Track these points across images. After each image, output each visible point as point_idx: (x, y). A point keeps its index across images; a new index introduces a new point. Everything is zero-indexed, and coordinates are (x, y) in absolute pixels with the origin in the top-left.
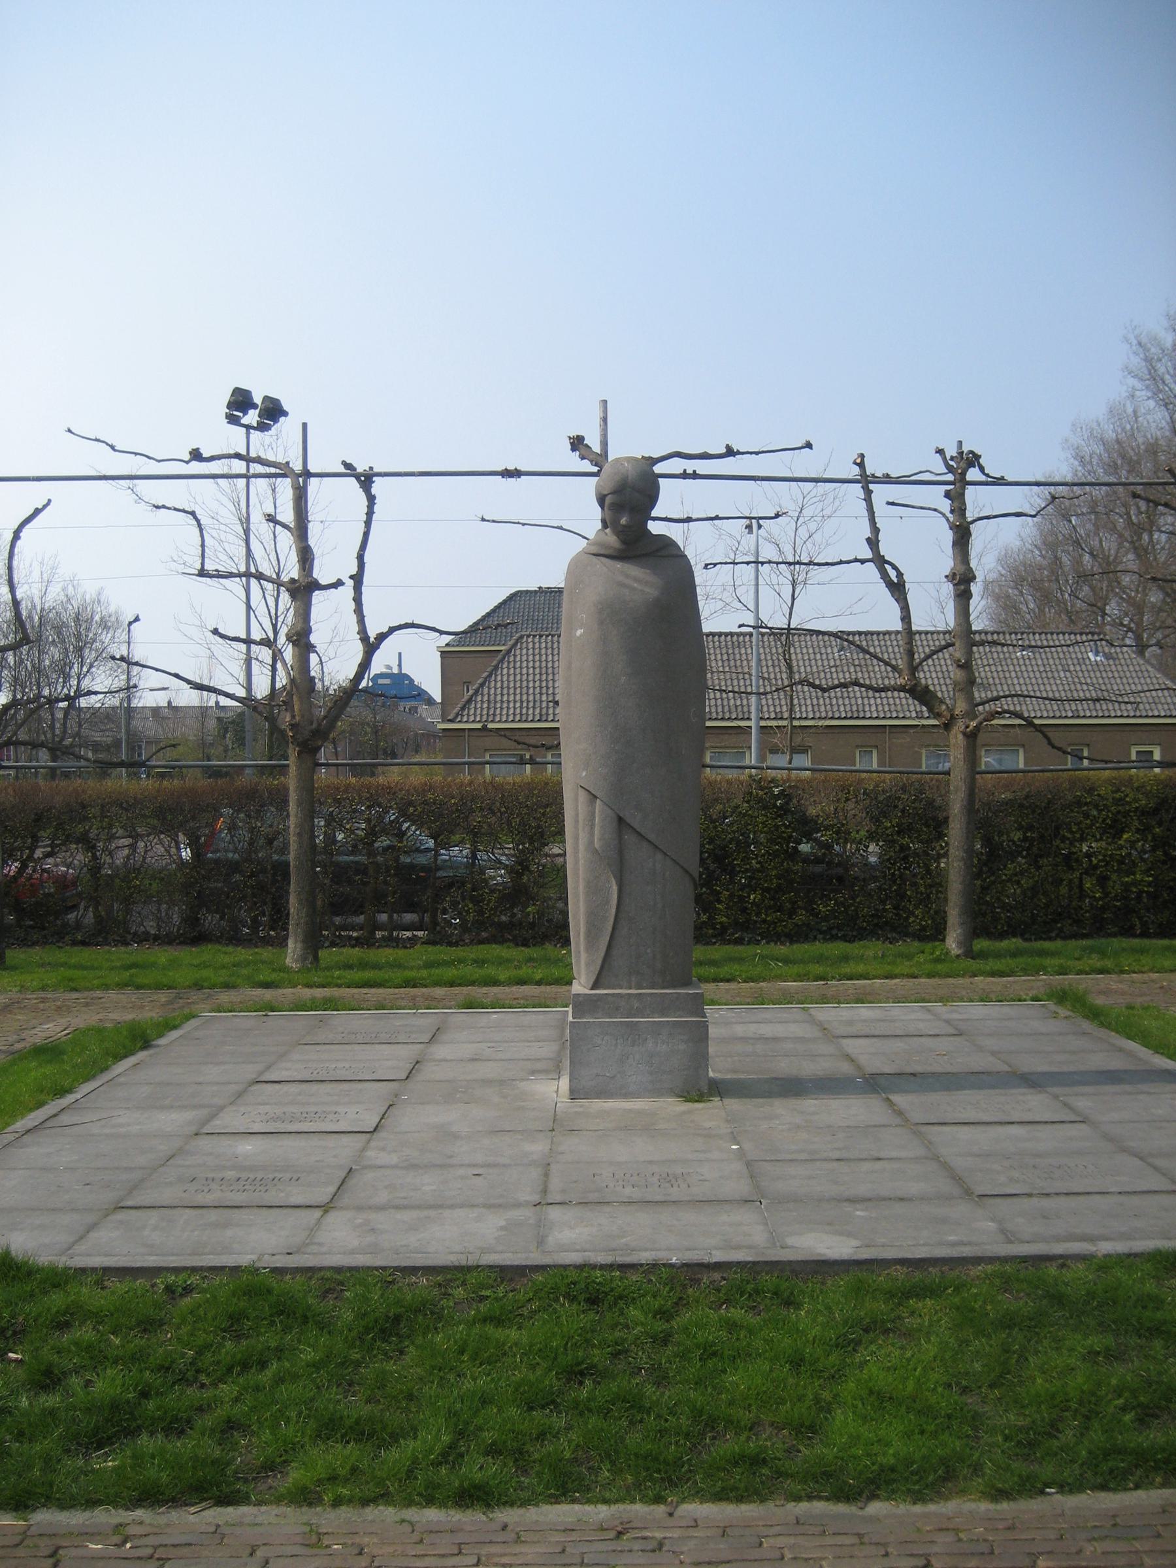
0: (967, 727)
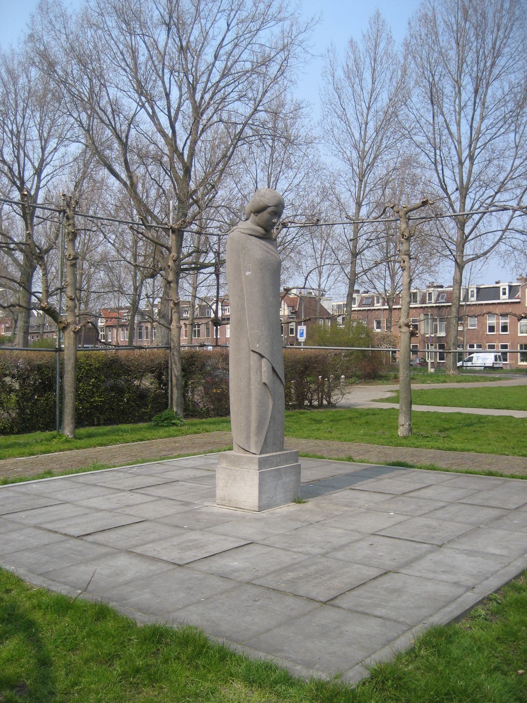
0: (76, 329)
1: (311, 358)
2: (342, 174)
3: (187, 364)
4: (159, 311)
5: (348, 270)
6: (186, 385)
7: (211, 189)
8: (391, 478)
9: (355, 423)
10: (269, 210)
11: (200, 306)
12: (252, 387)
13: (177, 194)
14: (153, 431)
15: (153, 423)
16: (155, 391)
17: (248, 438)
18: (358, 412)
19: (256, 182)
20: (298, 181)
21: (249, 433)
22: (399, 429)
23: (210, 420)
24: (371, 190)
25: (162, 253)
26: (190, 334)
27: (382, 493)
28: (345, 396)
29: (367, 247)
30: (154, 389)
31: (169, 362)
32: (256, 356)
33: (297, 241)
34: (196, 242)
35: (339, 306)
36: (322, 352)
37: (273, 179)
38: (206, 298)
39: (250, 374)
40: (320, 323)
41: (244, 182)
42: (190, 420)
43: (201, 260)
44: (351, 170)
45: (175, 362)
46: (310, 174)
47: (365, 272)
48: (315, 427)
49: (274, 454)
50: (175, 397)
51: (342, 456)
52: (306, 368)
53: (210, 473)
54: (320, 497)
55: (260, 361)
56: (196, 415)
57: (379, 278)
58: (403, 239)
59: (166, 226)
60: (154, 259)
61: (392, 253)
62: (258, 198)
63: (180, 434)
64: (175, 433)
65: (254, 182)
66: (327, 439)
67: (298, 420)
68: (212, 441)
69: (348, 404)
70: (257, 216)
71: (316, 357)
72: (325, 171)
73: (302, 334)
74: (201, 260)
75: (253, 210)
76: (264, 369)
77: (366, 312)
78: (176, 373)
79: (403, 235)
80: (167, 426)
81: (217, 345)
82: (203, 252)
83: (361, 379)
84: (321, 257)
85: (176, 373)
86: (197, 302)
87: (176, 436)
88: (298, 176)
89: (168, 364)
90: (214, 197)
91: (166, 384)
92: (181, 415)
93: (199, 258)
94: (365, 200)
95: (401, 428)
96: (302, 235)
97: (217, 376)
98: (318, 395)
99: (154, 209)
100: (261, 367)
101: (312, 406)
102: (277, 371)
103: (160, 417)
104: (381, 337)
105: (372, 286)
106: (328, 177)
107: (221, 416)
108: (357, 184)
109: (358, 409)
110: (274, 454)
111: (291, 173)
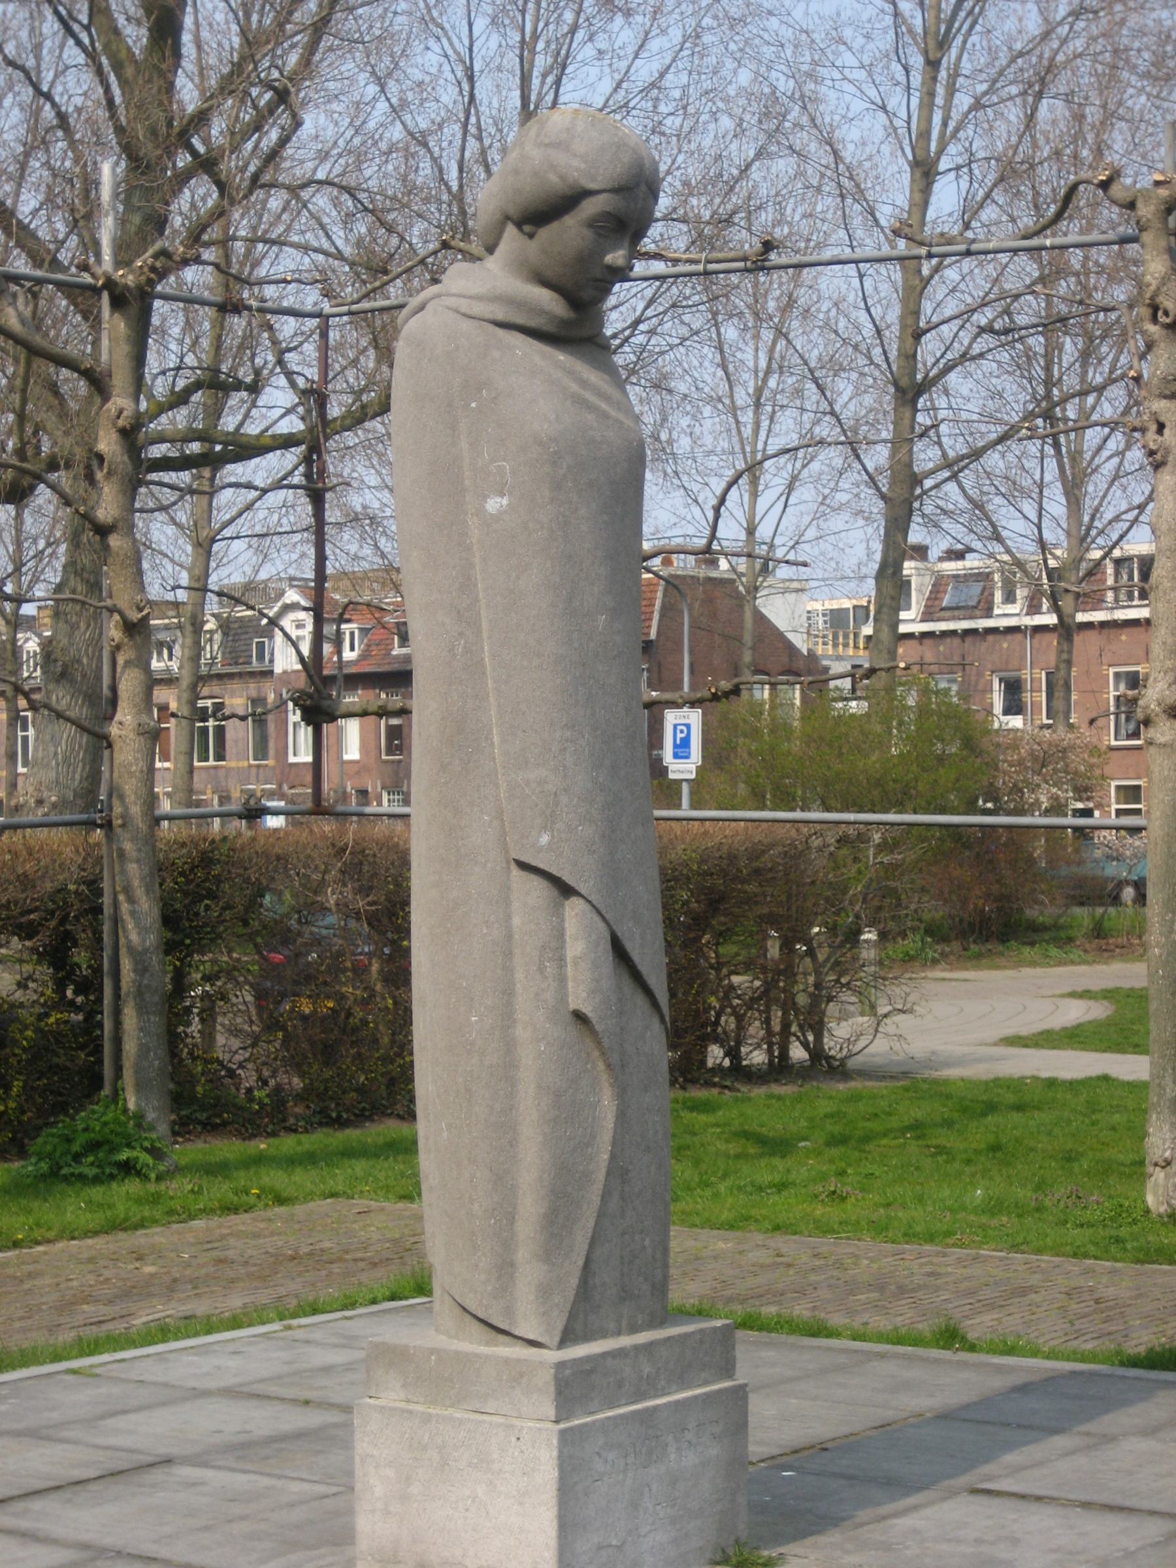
1: (732, 857)
2: (848, 33)
3: (186, 894)
4: (47, 646)
5: (878, 457)
6: (180, 986)
7: (271, 109)
8: (1149, 1432)
9: (941, 1150)
10: (590, 208)
11: (226, 625)
12: (521, 1033)
13: (119, 130)
14: (35, 1205)
15: (28, 1167)
16: (41, 1017)
17: (505, 1269)
18: (949, 1097)
19: (471, 79)
20: (656, 66)
21: (507, 1244)
22: (1150, 1184)
23: (288, 1144)
24: (978, 105)
25: (54, 389)
26: (184, 747)
27: (1121, 1509)
28: (889, 1026)
29: (965, 357)
30: (38, 1010)
31: (106, 885)
32: (538, 889)
33: (652, 332)
34: (205, 343)
35: (837, 618)
36: (781, 832)
37: (541, 62)
38: (249, 587)
39: (509, 970)
40: (757, 694)
41: (417, 75)
42: (200, 1145)
43: (229, 423)
44: (889, 20)
45: (127, 890)
46: (707, 39)
47: (953, 467)
48: (766, 1171)
49: (626, 1341)
50: (130, 1047)
51: (903, 1317)
52: (715, 901)
53: (313, 1419)
54: (833, 1537)
55: (557, 911)
56: (225, 1124)
57: (1013, 492)
58: (1152, 328)
59: (87, 278)
60: (21, 417)
61: (1071, 382)
62: (535, 154)
63: (158, 1215)
64: (136, 1213)
65: (459, 74)
66: (824, 1228)
67: (688, 1139)
68: (305, 1250)
69: (901, 1057)
70: (531, 236)
71: (756, 853)
72: (774, 23)
73: (682, 749)
74: (229, 423)
75: (513, 211)
76: (575, 948)
77: (956, 641)
78: (134, 937)
79: (1155, 308)
80: (96, 1180)
81: (319, 808)
82: (238, 386)
83: (945, 939)
84: (758, 405)
85: (134, 937)
86: (212, 605)
87: (141, 1225)
88: (654, 45)
89: (99, 893)
90: (284, 141)
91: (90, 986)
92: (163, 1128)
93: (215, 412)
94: (952, 149)
95: (1159, 1175)
96: (674, 306)
97: (317, 941)
98: (767, 1021)
99: (17, 194)
100: (560, 935)
101: (740, 1072)
102: (636, 956)
103: (69, 1140)
104: (1032, 753)
105: (983, 527)
106: (789, 51)
107: (340, 1123)
108: (916, 79)
109: (946, 1082)
110: (626, 1341)
111: (623, 33)
